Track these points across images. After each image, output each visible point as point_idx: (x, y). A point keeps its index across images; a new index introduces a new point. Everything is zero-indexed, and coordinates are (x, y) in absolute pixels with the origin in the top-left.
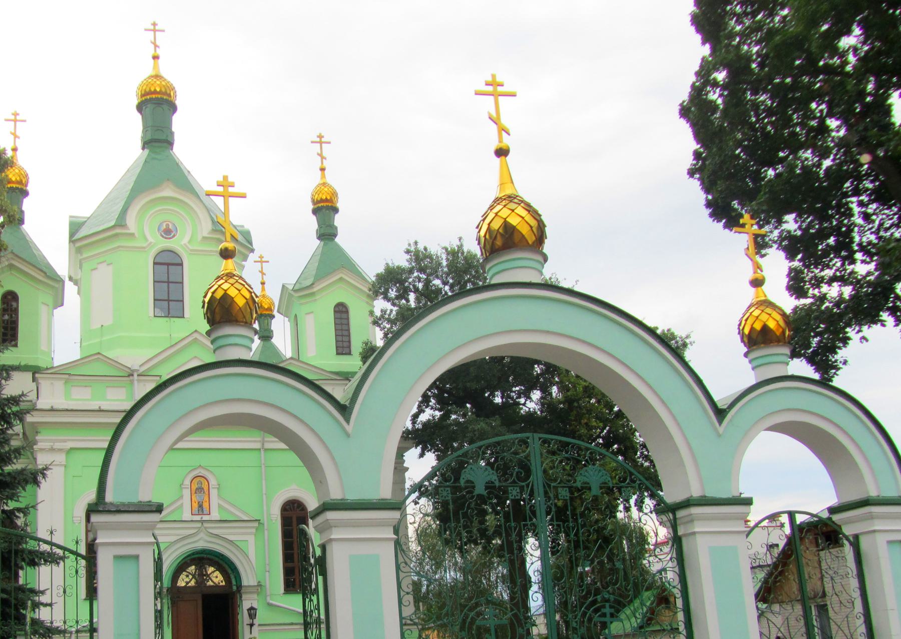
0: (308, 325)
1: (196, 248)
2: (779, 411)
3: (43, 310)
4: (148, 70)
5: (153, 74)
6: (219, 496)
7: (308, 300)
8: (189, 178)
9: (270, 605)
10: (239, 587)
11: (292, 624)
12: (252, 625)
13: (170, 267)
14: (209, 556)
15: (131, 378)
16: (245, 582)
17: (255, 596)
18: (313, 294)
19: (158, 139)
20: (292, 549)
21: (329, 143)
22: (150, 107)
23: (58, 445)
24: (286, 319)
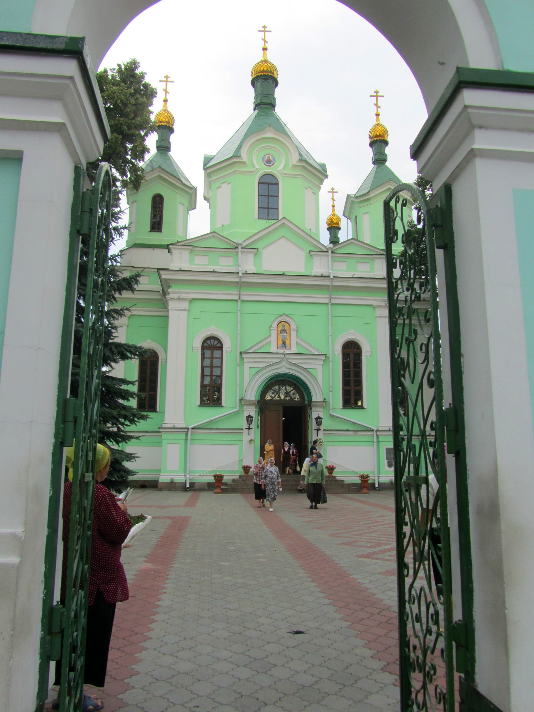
0: (365, 223)
1: (287, 173)
2: (379, 464)
3: (181, 210)
4: (259, 57)
5: (263, 59)
6: (297, 336)
7: (365, 204)
8: (285, 128)
9: (332, 416)
10: (310, 401)
11: (348, 430)
12: (318, 430)
14: (289, 379)
15: (237, 250)
16: (314, 399)
17: (321, 409)
18: (369, 199)
19: (265, 104)
20: (349, 368)
22: (260, 81)
23: (183, 296)
24: (349, 221)
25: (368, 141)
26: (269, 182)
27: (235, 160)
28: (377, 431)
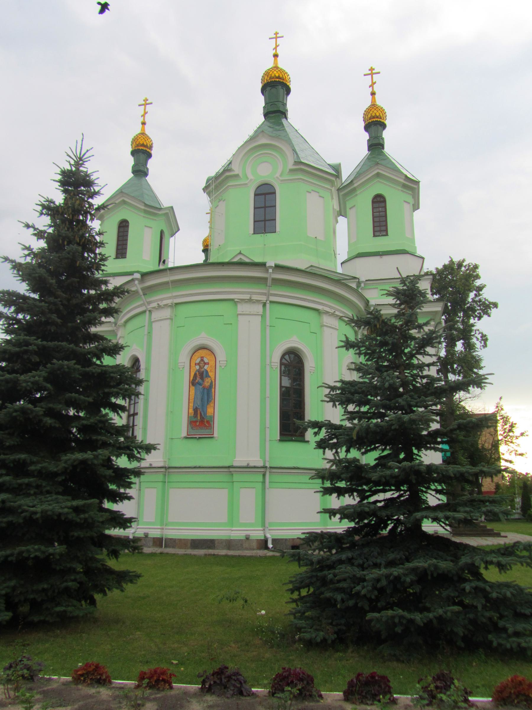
5: (274, 66)
13: (267, 196)
18: (354, 190)
19: (275, 112)
21: (379, 73)
22: (268, 89)
25: (363, 124)
26: (265, 192)
27: (228, 174)
28: (271, 468)
